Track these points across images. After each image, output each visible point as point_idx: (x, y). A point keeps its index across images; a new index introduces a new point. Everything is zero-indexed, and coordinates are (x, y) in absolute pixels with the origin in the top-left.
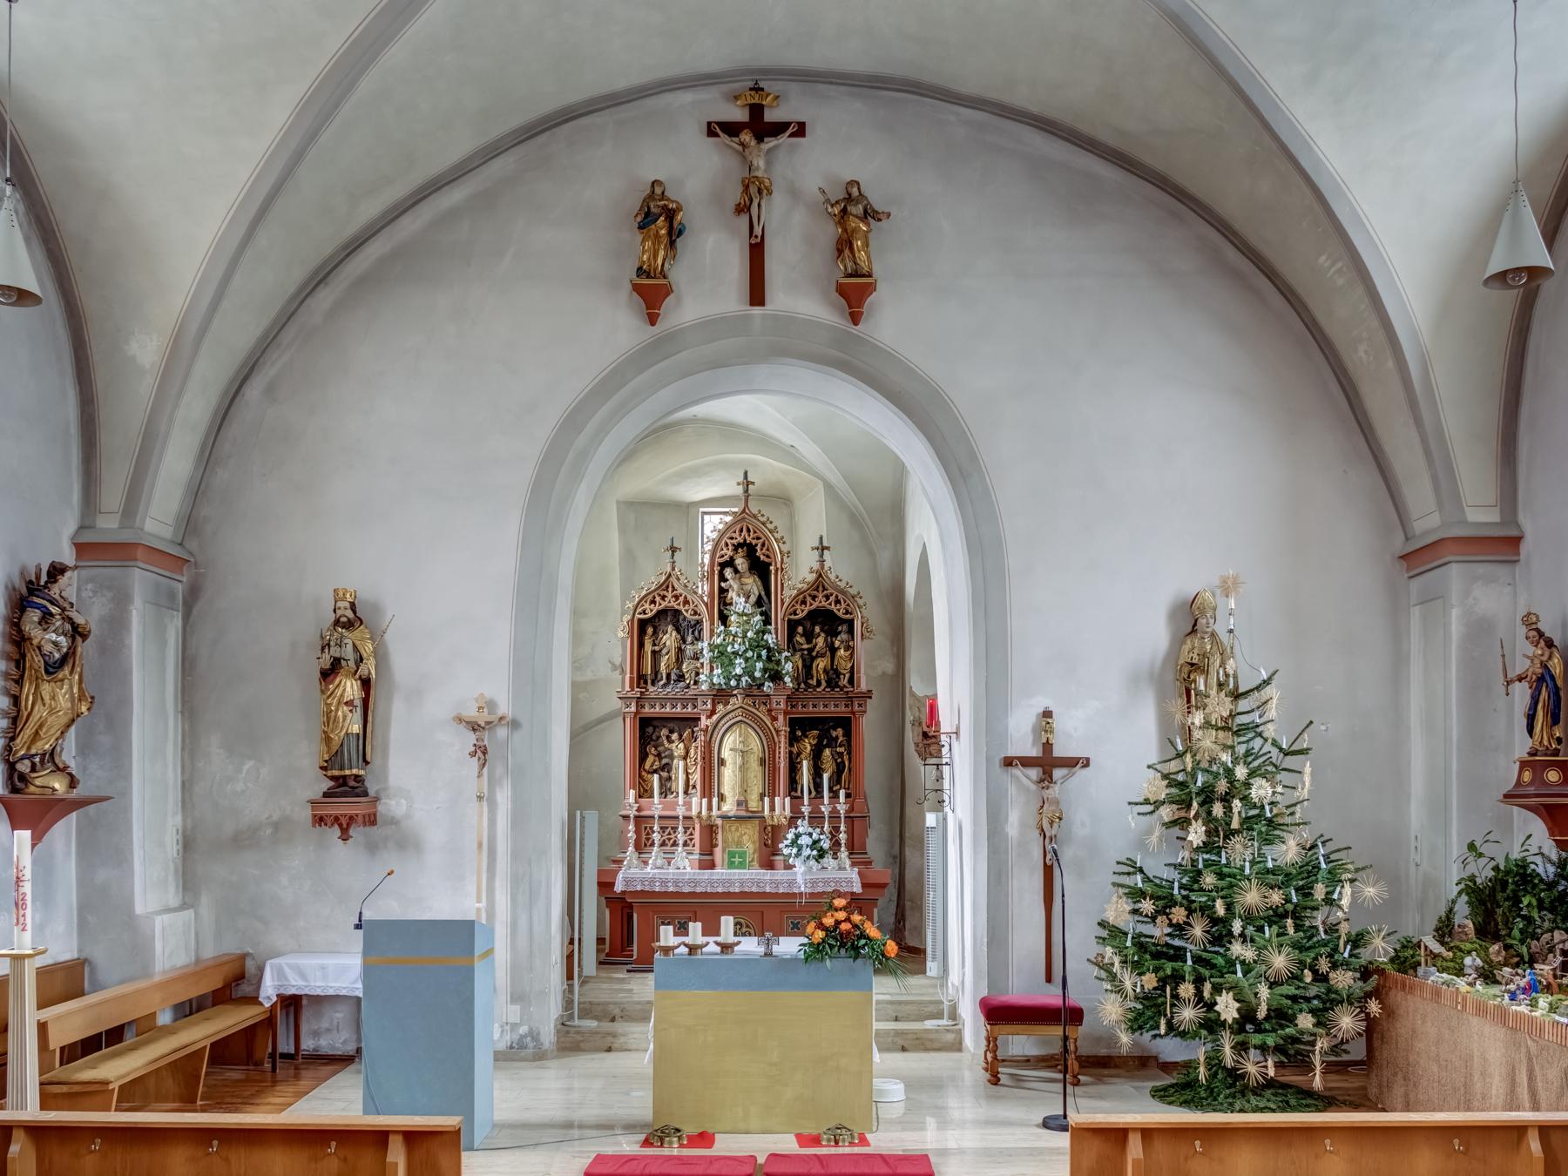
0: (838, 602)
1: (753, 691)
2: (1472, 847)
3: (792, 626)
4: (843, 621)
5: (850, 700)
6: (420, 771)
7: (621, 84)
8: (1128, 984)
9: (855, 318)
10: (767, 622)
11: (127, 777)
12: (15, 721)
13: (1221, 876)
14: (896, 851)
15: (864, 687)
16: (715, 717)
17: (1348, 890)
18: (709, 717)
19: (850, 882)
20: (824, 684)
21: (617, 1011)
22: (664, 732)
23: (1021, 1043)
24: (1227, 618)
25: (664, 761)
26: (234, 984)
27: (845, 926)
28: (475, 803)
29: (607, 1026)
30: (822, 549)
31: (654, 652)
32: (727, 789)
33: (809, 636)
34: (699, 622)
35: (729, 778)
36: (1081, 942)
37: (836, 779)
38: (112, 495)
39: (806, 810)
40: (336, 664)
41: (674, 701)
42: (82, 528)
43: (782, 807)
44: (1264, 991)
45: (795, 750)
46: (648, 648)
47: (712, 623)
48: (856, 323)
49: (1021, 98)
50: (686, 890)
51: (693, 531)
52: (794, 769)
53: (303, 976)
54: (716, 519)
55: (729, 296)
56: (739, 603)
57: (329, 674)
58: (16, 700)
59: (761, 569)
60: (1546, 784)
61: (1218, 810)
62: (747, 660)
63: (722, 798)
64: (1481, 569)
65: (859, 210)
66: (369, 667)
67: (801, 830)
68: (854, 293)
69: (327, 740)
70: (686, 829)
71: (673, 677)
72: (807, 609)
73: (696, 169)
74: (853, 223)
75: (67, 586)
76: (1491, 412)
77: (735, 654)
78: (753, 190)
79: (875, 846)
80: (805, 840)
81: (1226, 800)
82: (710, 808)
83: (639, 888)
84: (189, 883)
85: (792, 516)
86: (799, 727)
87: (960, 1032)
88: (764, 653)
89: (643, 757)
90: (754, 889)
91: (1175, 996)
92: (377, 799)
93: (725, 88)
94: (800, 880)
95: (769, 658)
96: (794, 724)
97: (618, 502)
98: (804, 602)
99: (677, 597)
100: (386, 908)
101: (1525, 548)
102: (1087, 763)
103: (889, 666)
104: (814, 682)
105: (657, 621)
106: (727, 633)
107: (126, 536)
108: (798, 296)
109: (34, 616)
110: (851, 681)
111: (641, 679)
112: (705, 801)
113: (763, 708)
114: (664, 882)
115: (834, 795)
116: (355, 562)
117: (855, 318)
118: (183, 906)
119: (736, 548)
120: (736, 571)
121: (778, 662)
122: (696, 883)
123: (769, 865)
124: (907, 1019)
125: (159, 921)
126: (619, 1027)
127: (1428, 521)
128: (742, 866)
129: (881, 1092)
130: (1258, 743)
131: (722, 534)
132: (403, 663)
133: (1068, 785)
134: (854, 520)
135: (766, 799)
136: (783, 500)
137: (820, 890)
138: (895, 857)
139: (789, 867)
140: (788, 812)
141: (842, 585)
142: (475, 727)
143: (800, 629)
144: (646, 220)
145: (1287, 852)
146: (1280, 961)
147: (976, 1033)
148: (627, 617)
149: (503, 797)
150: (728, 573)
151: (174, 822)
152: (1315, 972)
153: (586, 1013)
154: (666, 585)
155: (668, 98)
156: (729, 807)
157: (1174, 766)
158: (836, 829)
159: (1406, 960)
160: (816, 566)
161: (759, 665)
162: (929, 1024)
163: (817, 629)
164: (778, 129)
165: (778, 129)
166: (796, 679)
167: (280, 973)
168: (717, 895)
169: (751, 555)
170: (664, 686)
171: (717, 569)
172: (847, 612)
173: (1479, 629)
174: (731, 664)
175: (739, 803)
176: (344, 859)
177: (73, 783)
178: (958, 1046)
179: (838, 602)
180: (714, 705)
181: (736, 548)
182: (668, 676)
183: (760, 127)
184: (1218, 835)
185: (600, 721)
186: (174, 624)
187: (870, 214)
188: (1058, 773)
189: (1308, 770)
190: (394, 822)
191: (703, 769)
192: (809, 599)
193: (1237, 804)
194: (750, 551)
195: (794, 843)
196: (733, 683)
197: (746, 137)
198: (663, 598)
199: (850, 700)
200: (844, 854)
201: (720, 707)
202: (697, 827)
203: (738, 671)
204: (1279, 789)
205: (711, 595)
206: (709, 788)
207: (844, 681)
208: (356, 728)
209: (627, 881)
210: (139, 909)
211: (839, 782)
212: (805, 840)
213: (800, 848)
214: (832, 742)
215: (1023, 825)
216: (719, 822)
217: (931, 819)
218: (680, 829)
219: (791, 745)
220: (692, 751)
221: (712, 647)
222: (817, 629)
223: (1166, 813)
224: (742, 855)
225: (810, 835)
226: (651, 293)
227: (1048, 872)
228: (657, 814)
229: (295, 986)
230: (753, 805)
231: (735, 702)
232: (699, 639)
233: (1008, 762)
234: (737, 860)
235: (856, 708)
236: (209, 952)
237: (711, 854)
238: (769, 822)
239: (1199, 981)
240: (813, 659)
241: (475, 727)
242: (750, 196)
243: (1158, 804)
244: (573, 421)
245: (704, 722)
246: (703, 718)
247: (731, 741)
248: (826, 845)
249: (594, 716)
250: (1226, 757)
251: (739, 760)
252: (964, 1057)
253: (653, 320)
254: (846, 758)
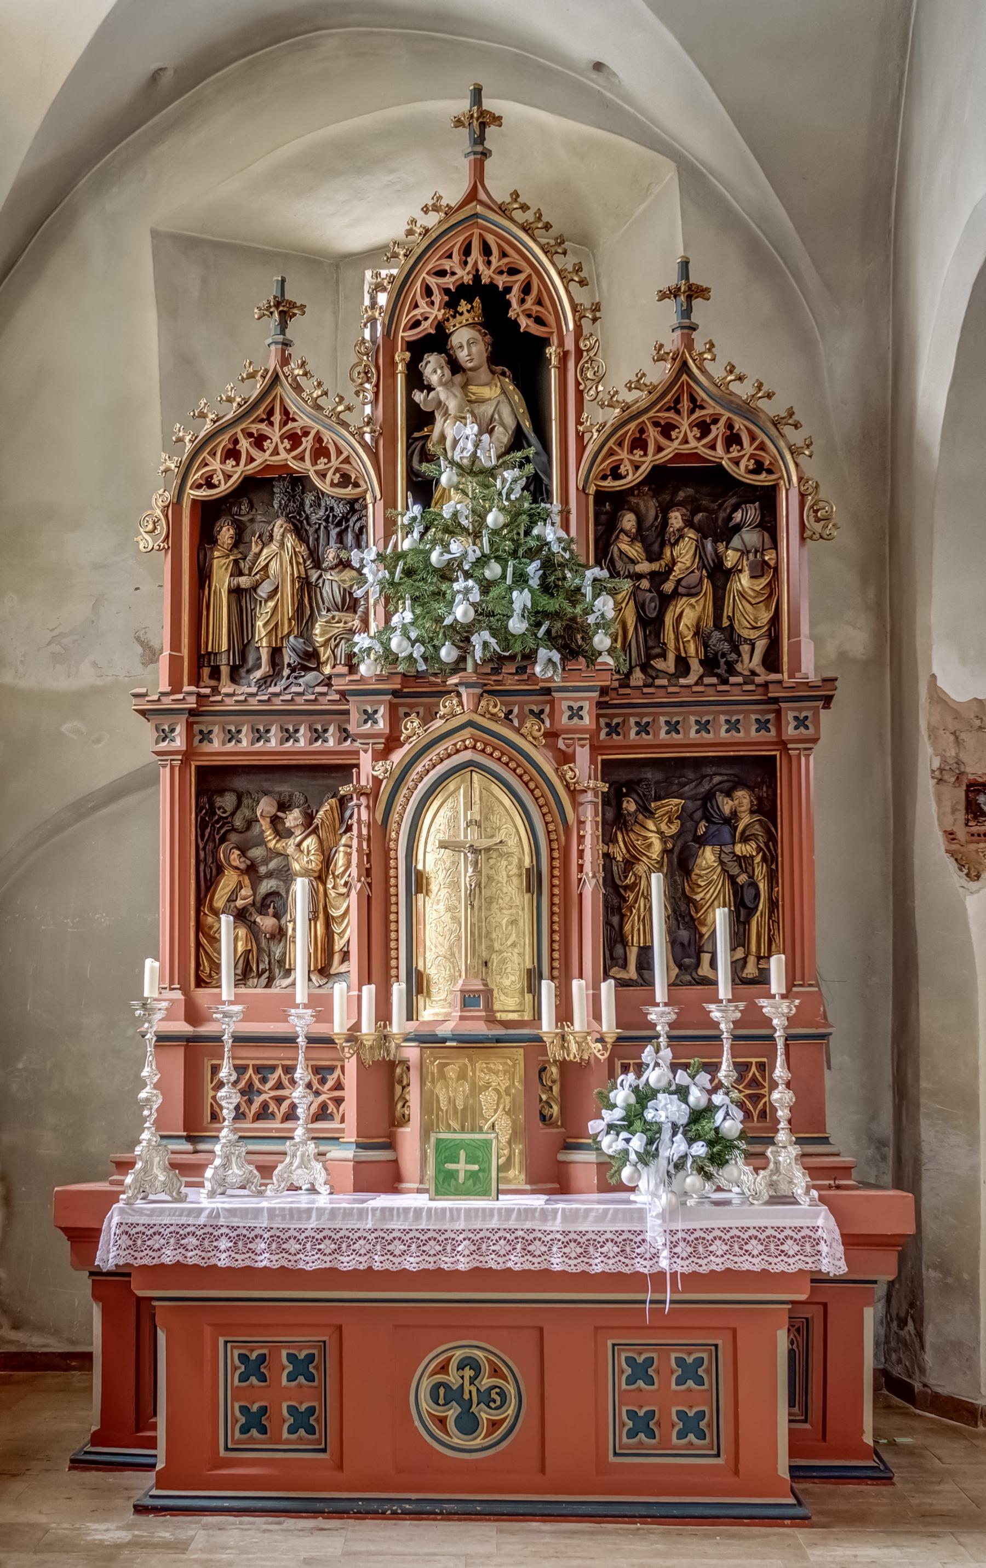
0: (733, 439)
3: (608, 507)
4: (750, 494)
10: (537, 488)
16: (397, 756)
18: (383, 754)
19: (810, 1239)
20: (695, 665)
22: (266, 806)
25: (266, 886)
31: (236, 592)
34: (355, 506)
35: (438, 924)
39: (660, 1016)
43: (588, 1014)
45: (619, 852)
46: (222, 580)
47: (390, 503)
50: (311, 1262)
52: (618, 897)
59: (520, 357)
62: (486, 586)
63: (418, 984)
67: (653, 1077)
70: (321, 1072)
71: (288, 657)
72: (649, 461)
80: (666, 1110)
82: (383, 1014)
83: (169, 1256)
86: (627, 787)
88: (533, 568)
90: (516, 1262)
94: (654, 1232)
95: (546, 588)
97: (155, 235)
98: (639, 443)
99: (295, 439)
104: (668, 665)
110: (772, 661)
111: (202, 664)
112: (369, 991)
113: (531, 725)
115: (750, 981)
119: (454, 298)
120: (455, 366)
121: (575, 595)
123: (556, 1181)
128: (477, 1185)
135: (547, 988)
137: (717, 1264)
138: (880, 1143)
139: (609, 1181)
140: (608, 1025)
141: (743, 390)
143: (628, 521)
154: (266, 406)
156: (438, 1011)
161: (521, 599)
163: (676, 519)
168: (403, 1278)
170: (265, 682)
171: (401, 357)
172: (759, 468)
175: (468, 1000)
179: (733, 439)
180: (395, 721)
181: (454, 298)
182: (276, 652)
185: (116, 792)
191: (367, 903)
192: (653, 434)
194: (490, 303)
195: (633, 1118)
196: (447, 653)
198: (259, 441)
200: (785, 1152)
201: (411, 725)
202: (351, 1066)
203: (461, 612)
206: (385, 954)
207: (752, 661)
209: (127, 1230)
212: (666, 1110)
213: (653, 1133)
216: (412, 1053)
218: (301, 1073)
219: (609, 839)
220: (340, 859)
221: (386, 560)
222: (676, 519)
224: (478, 1153)
225: (682, 1093)
230: (509, 1003)
231: (458, 707)
234: (462, 1167)
235: (790, 731)
237: (390, 1144)
238: (555, 1052)
240: (666, 600)
245: (369, 768)
246: (365, 759)
247: (440, 822)
248: (731, 1126)
249: (101, 781)
251: (466, 876)
254: (760, 872)
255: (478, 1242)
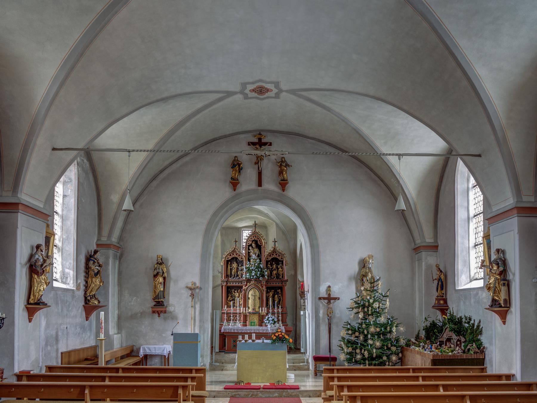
0: (279, 256)
1: (257, 280)
2: (425, 318)
3: (267, 262)
4: (281, 261)
5: (282, 282)
6: (177, 300)
7: (228, 133)
8: (345, 350)
9: (283, 190)
10: (261, 261)
11: (108, 301)
12: (86, 287)
13: (366, 325)
14: (295, 323)
15: (286, 279)
17: (395, 328)
21: (224, 361)
23: (323, 366)
24: (372, 264)
26: (131, 352)
27: (280, 336)
28: (190, 308)
29: (221, 365)
30: (275, 242)
32: (250, 306)
33: (272, 265)
34: (243, 261)
36: (336, 342)
37: (279, 303)
38: (105, 232)
39: (271, 311)
40: (158, 273)
41: (236, 282)
42: (98, 240)
43: (264, 311)
44: (374, 350)
46: (229, 268)
48: (284, 191)
49: (323, 138)
50: (240, 332)
51: (240, 236)
52: (267, 300)
53: (150, 350)
54: (247, 232)
55: (253, 185)
56: (254, 256)
57: (155, 276)
58: (87, 282)
59: (259, 247)
60: (440, 304)
61: (366, 310)
63: (249, 308)
64: (429, 253)
65: (284, 164)
66: (166, 275)
68: (283, 184)
69: (155, 292)
73: (244, 152)
74: (283, 167)
75: (98, 256)
76: (432, 215)
77: (252, 270)
78: (259, 159)
79: (289, 321)
80: (270, 319)
81: (368, 308)
82: (246, 311)
84: (120, 328)
85: (267, 231)
86: (269, 289)
87: (309, 366)
89: (227, 297)
91: (356, 353)
92: (166, 307)
93: (252, 134)
94: (269, 329)
96: (268, 288)
98: (270, 256)
100: (175, 331)
101: (439, 248)
102: (339, 299)
103: (293, 273)
105: (232, 260)
106: (250, 264)
107: (108, 242)
108: (270, 185)
109: (92, 262)
110: (283, 277)
111: (227, 276)
114: (234, 330)
115: (278, 308)
116: (164, 248)
117: (283, 190)
118: (118, 333)
119: (252, 241)
121: (264, 272)
122: (243, 330)
124: (296, 363)
125: (115, 336)
126: (224, 365)
127: (418, 241)
128: (254, 325)
129: (289, 376)
130: (377, 294)
131: (249, 237)
132: (173, 273)
133: (335, 305)
134: (283, 233)
136: (264, 227)
142: (191, 289)
144: (233, 166)
145: (382, 320)
146: (378, 344)
147: (312, 365)
148: (223, 260)
149: (198, 307)
150: (250, 248)
151: (116, 312)
152: (387, 346)
153: (216, 362)
154: (234, 251)
155: (238, 136)
157: (357, 299)
158: (279, 316)
159: (408, 345)
160: (273, 246)
161: (259, 273)
162: (301, 364)
164: (265, 144)
165: (265, 144)
166: (268, 276)
167: (144, 349)
169: (256, 243)
173: (429, 267)
174: (251, 272)
175: (253, 309)
176: (157, 320)
177: (99, 302)
178: (308, 369)
181: (252, 241)
183: (260, 143)
184: (366, 314)
186: (117, 263)
187: (287, 165)
188: (332, 301)
189: (388, 300)
190: (170, 312)
193: (370, 308)
194: (256, 242)
195: (268, 319)
197: (258, 146)
199: (282, 282)
200: (280, 322)
204: (381, 305)
205: (246, 254)
206: (245, 305)
207: (281, 277)
208: (162, 289)
210: (110, 333)
211: (279, 304)
212: (270, 319)
213: (269, 321)
214: (278, 293)
215: (323, 313)
217: (302, 313)
221: (246, 268)
223: (355, 311)
224: (254, 323)
226: (234, 183)
227: (330, 324)
228: (232, 312)
229: (148, 352)
230: (257, 310)
231: (252, 282)
232: (242, 265)
233: (320, 298)
236: (124, 345)
237: (246, 323)
239: (361, 349)
240: (273, 271)
241: (191, 289)
242: (259, 160)
243: (353, 308)
244: (215, 214)
245: (244, 288)
247: (251, 293)
248: (276, 320)
250: (368, 298)
251: (253, 298)
252: (310, 372)
253: (235, 190)
255: (254, 330)
